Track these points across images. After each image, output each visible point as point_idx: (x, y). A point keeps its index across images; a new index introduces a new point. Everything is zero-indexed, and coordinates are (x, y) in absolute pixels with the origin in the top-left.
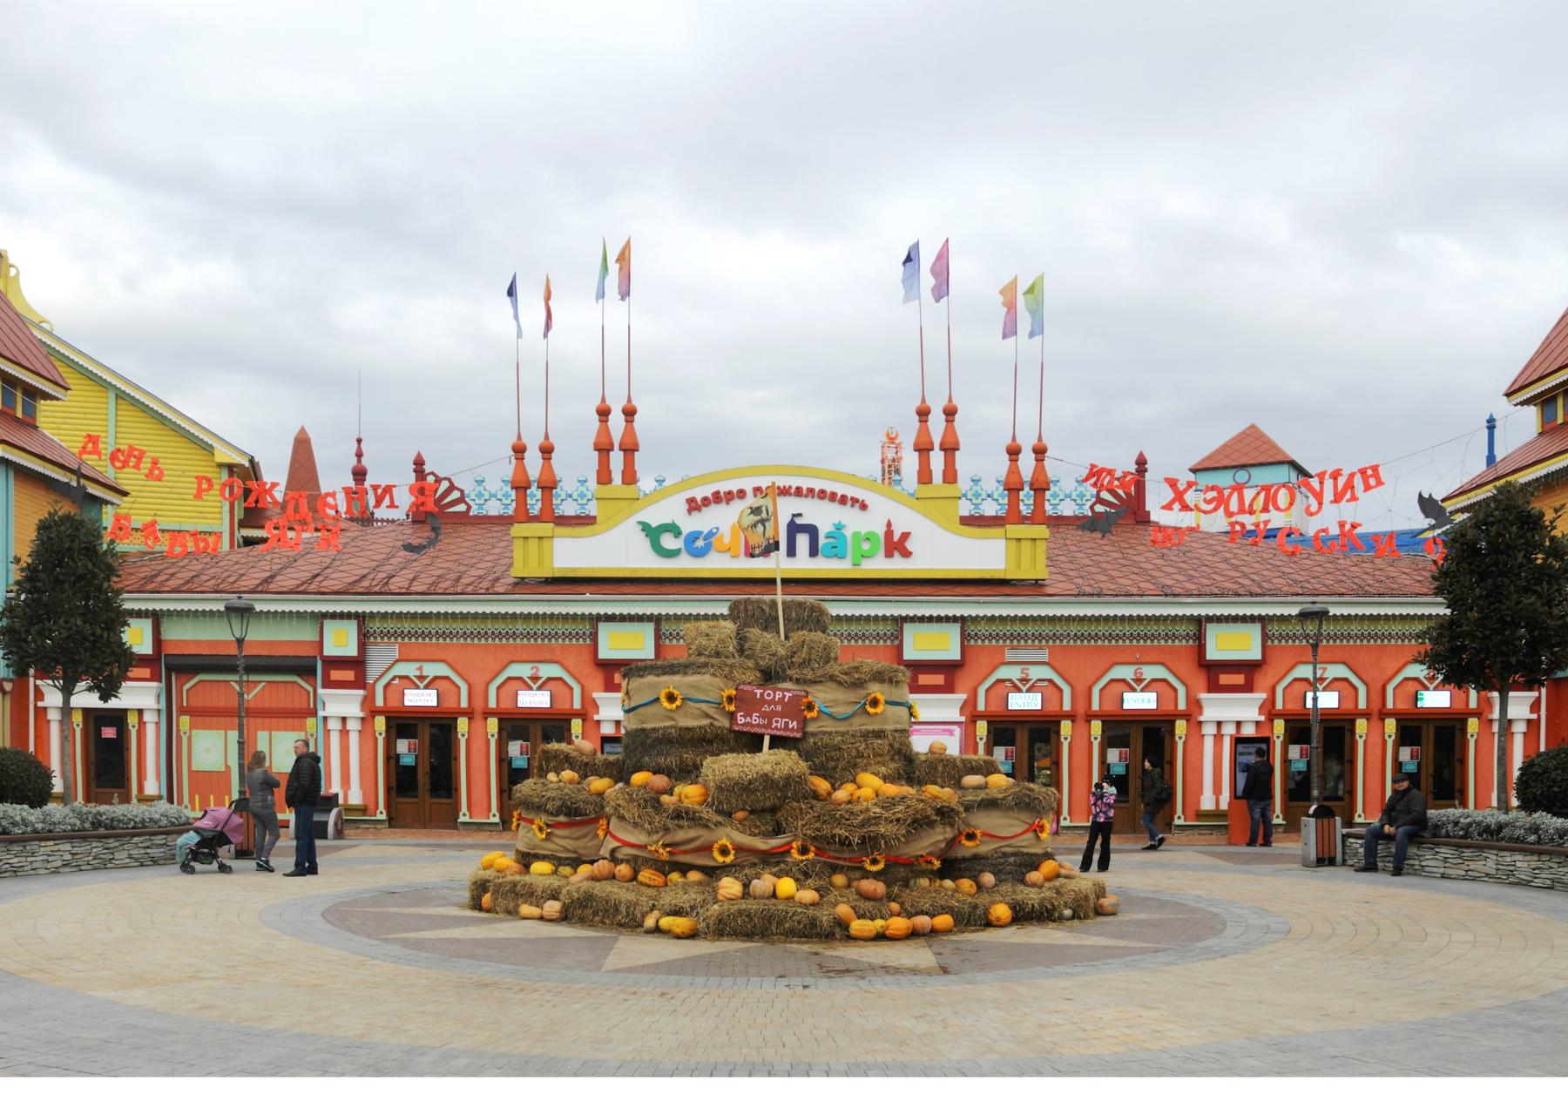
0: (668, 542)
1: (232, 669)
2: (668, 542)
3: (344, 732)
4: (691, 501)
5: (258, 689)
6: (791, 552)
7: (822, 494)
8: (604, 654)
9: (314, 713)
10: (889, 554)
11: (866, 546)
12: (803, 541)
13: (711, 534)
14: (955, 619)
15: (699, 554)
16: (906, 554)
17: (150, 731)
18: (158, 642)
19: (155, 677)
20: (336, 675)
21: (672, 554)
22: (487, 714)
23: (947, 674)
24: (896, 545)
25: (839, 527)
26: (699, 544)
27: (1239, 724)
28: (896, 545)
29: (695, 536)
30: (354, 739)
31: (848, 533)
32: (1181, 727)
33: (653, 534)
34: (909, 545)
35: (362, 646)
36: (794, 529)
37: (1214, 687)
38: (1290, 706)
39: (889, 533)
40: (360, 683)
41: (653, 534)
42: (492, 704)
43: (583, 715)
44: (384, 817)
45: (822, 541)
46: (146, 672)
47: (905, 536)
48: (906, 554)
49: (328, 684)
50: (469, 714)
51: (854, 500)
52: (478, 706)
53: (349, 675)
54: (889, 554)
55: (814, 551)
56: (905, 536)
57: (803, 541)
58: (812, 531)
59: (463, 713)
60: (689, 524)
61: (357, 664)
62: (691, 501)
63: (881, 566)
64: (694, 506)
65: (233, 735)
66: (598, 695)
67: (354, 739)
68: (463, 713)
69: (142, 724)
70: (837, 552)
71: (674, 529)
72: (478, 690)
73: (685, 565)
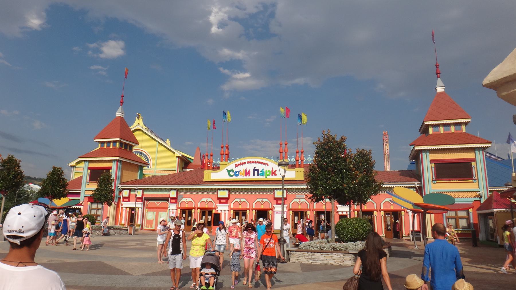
0: (232, 173)
1: (167, 200)
2: (232, 173)
3: (225, 213)
4: (236, 165)
5: (158, 204)
6: (254, 175)
7: (258, 162)
8: (276, 196)
9: (167, 208)
10: (272, 175)
11: (268, 173)
12: (256, 172)
13: (239, 172)
14: (226, 189)
15: (237, 176)
16: (276, 175)
17: (140, 212)
18: (143, 195)
19: (142, 201)
20: (172, 201)
21: (232, 176)
22: (253, 209)
23: (175, 200)
24: (274, 173)
25: (263, 169)
26: (237, 174)
27: (342, 212)
28: (274, 173)
29: (236, 172)
30: (227, 214)
31: (265, 171)
32: (270, 211)
33: (229, 171)
34: (276, 173)
35: (177, 195)
36: (255, 170)
37: (220, 203)
38: (385, 208)
39: (272, 170)
40: (176, 202)
41: (229, 171)
42: (254, 207)
43: (215, 209)
44: (384, 235)
45: (260, 172)
46: (140, 200)
47: (275, 171)
48: (276, 175)
49: (171, 203)
50: (195, 208)
51: (266, 164)
52: (196, 207)
53: (174, 201)
54: (272, 175)
55: (258, 175)
56: (275, 171)
57: (256, 172)
58: (258, 170)
59: (375, 210)
60: (235, 169)
61: (175, 198)
62: (236, 165)
63: (271, 177)
64: (237, 166)
65: (155, 213)
66: (275, 205)
67: (227, 214)
68: (375, 210)
69: (139, 210)
70: (263, 175)
71: (232, 171)
72: (251, 203)
73: (234, 178)
